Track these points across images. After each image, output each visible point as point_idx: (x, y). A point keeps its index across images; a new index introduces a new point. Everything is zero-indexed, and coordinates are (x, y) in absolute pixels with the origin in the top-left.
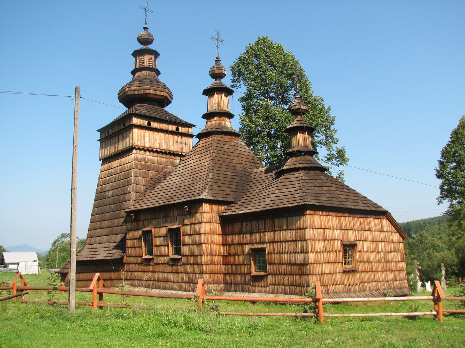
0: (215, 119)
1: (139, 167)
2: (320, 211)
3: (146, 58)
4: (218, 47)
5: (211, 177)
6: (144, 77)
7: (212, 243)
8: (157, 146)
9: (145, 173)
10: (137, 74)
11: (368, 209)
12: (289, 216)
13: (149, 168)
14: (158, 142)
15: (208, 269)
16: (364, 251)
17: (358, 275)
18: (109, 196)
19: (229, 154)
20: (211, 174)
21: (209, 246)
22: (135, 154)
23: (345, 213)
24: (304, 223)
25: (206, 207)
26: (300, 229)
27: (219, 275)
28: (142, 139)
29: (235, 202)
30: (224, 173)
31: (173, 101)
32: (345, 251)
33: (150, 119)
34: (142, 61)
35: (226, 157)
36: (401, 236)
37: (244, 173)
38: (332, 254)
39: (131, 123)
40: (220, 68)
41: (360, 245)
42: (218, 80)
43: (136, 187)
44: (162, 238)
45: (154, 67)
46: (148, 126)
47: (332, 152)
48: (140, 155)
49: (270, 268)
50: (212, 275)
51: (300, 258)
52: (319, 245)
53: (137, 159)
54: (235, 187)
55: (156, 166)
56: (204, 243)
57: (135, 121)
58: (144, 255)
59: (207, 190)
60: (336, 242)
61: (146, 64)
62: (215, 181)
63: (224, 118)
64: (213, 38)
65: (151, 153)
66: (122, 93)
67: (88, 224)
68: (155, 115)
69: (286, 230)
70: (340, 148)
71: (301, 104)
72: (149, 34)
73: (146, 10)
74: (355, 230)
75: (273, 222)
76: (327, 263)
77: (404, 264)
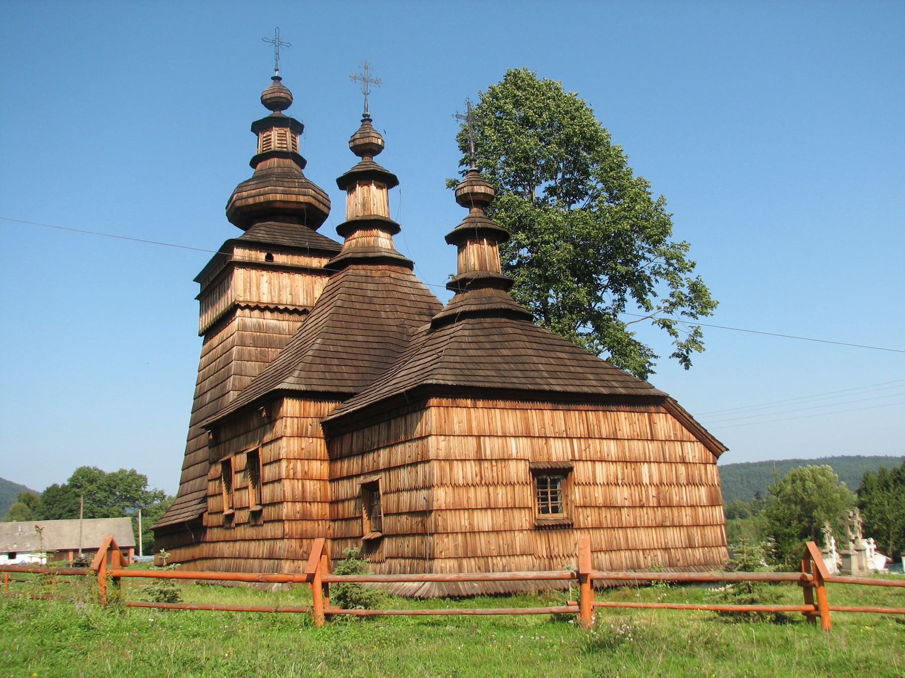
0: (358, 234)
1: (249, 341)
2: (466, 398)
3: (274, 134)
4: (366, 94)
5: (316, 347)
7: (306, 477)
8: (286, 299)
9: (261, 353)
10: (259, 166)
11: (604, 391)
12: (408, 413)
13: (270, 344)
14: (288, 292)
15: (297, 529)
16: (595, 484)
17: (577, 535)
19: (375, 300)
20: (319, 341)
21: (298, 485)
22: (241, 316)
24: (426, 424)
25: (290, 406)
26: (422, 438)
28: (254, 289)
29: (355, 394)
30: (351, 338)
33: (271, 248)
34: (268, 141)
35: (365, 306)
36: (710, 450)
37: (399, 336)
38: (501, 491)
40: (366, 135)
41: (581, 471)
42: (367, 159)
44: (242, 474)
45: (291, 150)
47: (681, 289)
50: (304, 541)
51: (419, 499)
52: (465, 472)
54: (366, 364)
56: (288, 478)
57: (239, 254)
58: (225, 508)
59: (296, 373)
60: (512, 465)
61: (275, 145)
62: (322, 355)
63: (375, 232)
64: (355, 78)
65: (276, 314)
67: (182, 457)
68: (286, 241)
69: (404, 442)
70: (694, 280)
71: (474, 183)
72: (282, 89)
73: (277, 43)
74: (571, 438)
75: (389, 427)
76: (486, 509)
77: (718, 513)
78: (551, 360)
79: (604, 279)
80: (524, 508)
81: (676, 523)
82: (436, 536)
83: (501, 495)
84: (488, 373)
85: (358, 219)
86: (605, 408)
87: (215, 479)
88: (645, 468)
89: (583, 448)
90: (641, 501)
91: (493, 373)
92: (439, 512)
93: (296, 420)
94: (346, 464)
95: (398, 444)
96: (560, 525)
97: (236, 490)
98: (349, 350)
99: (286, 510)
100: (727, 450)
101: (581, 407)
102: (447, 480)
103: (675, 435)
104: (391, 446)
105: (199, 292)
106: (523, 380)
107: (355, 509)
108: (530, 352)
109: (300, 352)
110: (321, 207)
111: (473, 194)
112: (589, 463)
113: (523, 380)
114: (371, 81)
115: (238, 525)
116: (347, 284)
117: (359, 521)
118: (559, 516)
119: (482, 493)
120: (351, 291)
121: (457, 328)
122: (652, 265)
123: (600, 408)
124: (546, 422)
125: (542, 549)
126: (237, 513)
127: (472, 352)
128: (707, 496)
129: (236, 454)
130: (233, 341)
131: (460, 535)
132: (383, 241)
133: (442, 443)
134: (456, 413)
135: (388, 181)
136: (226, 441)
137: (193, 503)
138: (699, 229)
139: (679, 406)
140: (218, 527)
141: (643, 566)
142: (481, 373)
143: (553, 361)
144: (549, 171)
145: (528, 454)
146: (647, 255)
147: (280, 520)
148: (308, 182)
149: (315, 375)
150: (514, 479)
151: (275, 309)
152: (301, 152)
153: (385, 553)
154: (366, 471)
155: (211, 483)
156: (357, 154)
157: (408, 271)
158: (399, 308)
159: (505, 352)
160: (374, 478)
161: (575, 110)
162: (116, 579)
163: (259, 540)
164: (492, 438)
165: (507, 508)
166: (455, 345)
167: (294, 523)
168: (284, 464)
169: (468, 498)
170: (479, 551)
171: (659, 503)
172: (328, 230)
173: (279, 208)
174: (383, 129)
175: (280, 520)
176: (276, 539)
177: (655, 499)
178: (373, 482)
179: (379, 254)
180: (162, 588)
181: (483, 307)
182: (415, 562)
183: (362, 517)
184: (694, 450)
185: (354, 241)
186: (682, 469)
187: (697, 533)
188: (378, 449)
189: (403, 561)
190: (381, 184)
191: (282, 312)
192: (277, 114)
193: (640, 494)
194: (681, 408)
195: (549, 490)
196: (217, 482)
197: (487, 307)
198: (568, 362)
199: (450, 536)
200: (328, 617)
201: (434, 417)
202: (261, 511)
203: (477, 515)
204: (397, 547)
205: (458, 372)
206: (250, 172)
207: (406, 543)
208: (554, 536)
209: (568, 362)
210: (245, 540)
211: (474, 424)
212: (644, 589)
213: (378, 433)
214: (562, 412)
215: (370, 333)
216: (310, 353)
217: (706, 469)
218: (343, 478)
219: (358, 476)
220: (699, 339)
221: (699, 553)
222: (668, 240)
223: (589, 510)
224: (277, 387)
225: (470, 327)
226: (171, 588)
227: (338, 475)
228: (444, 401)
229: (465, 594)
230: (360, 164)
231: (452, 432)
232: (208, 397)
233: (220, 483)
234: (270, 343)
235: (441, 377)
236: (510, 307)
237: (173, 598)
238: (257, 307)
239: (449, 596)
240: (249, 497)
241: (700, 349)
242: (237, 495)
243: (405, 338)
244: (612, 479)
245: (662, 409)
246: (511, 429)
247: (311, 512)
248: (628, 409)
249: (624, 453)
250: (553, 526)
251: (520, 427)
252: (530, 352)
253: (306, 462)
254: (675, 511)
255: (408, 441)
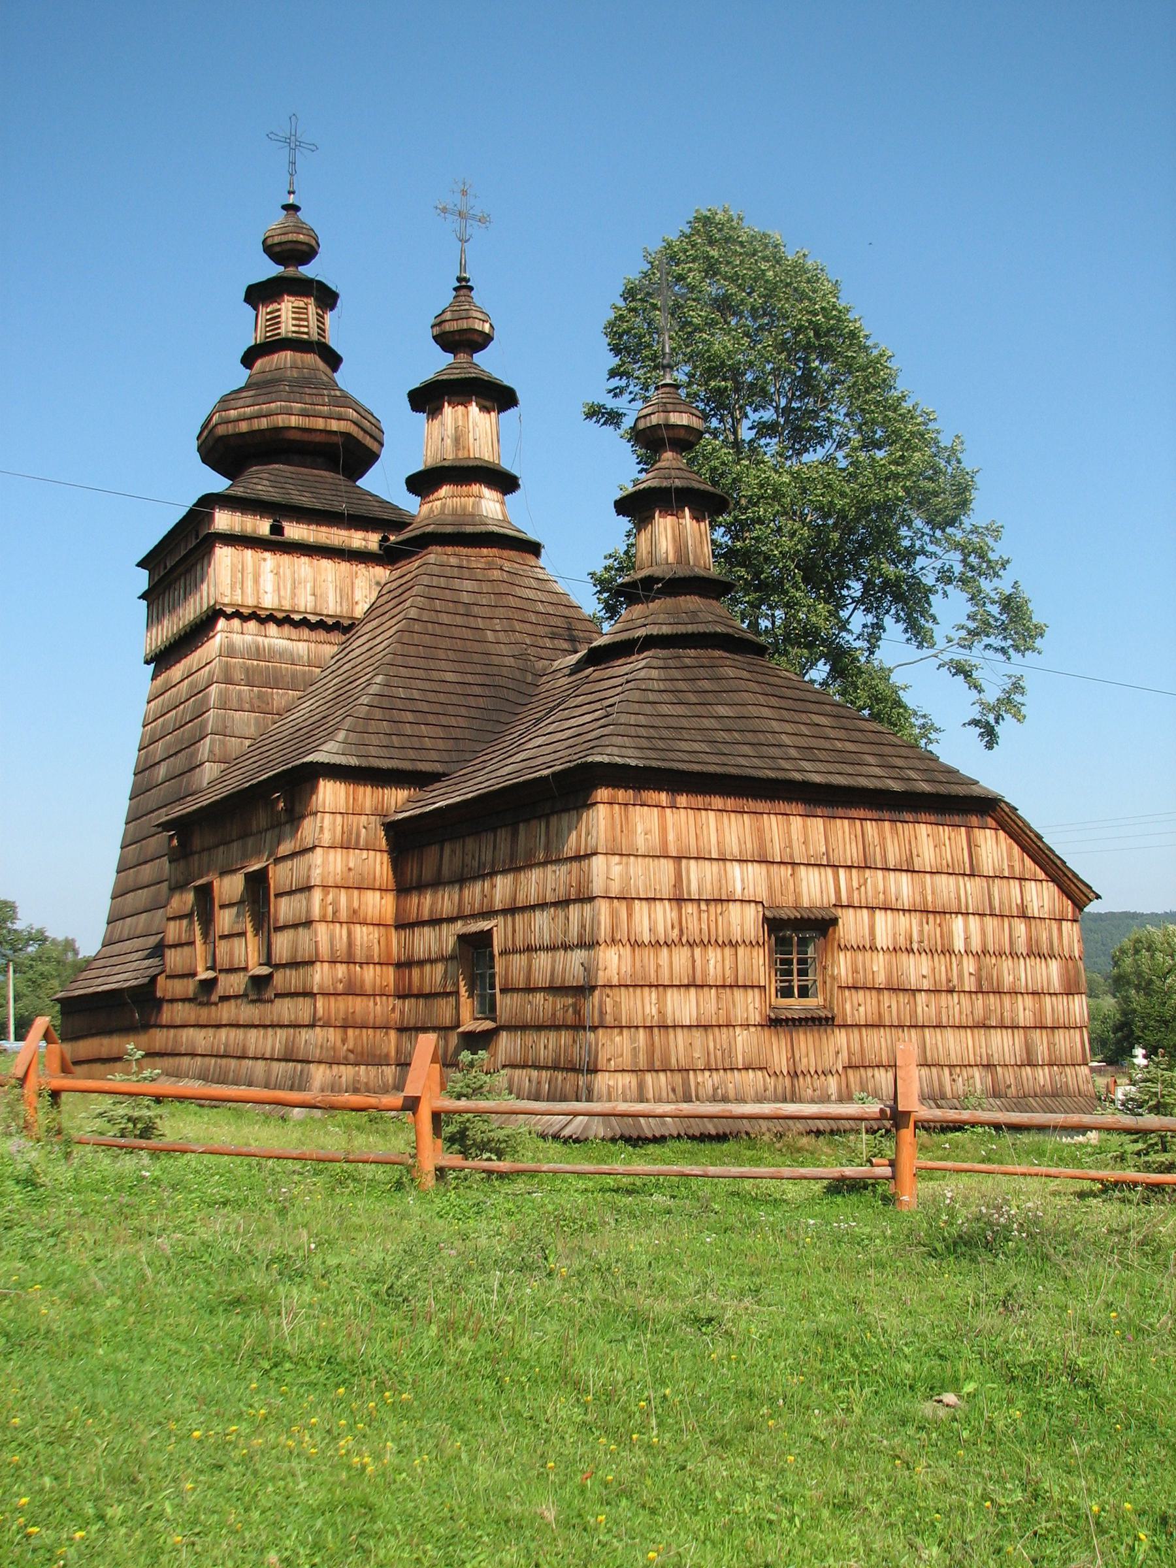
0: (445, 490)
1: (238, 675)
3: (287, 307)
4: (463, 241)
5: (374, 689)
6: (277, 374)
7: (356, 918)
8: (305, 603)
9: (260, 696)
10: (259, 364)
11: (896, 786)
12: (553, 813)
13: (275, 681)
16: (874, 948)
17: (840, 1038)
18: (160, 781)
19: (476, 610)
20: (379, 679)
21: (341, 932)
23: (789, 800)
24: (588, 834)
25: (329, 793)
26: (578, 858)
27: (380, 1034)
28: (249, 584)
29: (445, 775)
30: (435, 675)
31: (385, 453)
32: (782, 944)
34: (275, 320)
35: (459, 620)
36: (1069, 897)
37: (518, 675)
38: (713, 955)
39: (212, 531)
40: (464, 314)
41: (851, 926)
42: (463, 357)
43: (223, 743)
44: (234, 910)
45: (315, 337)
46: (273, 537)
48: (244, 635)
49: (506, 1005)
50: (350, 1031)
51: (572, 964)
53: (230, 651)
54: (462, 722)
55: (304, 673)
56: (323, 920)
57: (223, 520)
58: (200, 969)
59: (341, 736)
60: (734, 909)
61: (287, 327)
62: (385, 704)
63: (475, 488)
64: (444, 210)
66: (205, 434)
68: (305, 500)
69: (544, 864)
70: (1008, 591)
71: (670, 407)
72: (300, 227)
73: (293, 143)
75: (515, 834)
76: (687, 986)
78: (803, 727)
79: (856, 588)
80: (752, 987)
81: (1008, 1023)
82: (600, 1031)
83: (714, 963)
84: (696, 746)
85: (446, 464)
86: (895, 816)
87: (181, 917)
88: (958, 923)
89: (855, 885)
90: (949, 981)
91: (704, 747)
92: (608, 990)
93: (339, 817)
94: (428, 899)
95: (531, 866)
96: (813, 1019)
97: (222, 937)
98: (431, 697)
99: (320, 976)
100: (1098, 897)
101: (854, 813)
102: (622, 935)
103: (1011, 867)
104: (518, 870)
105: (146, 587)
106: (757, 762)
107: (445, 977)
108: (766, 712)
109: (342, 697)
110: (368, 441)
111: (669, 427)
112: (865, 911)
113: (757, 762)
114: (473, 217)
115: (225, 998)
116: (426, 580)
117: (452, 1000)
118: (810, 1002)
119: (681, 957)
120: (435, 593)
121: (638, 664)
122: (938, 564)
123: (887, 815)
124: (794, 837)
125: (779, 1058)
126: (222, 978)
127: (665, 709)
128: (1061, 976)
129: (223, 873)
130: (211, 674)
131: (641, 1031)
132: (489, 505)
133: (616, 866)
134: (642, 816)
135: (499, 398)
136: (203, 850)
137: (135, 956)
138: (1029, 498)
139: (1019, 817)
140: (183, 1000)
141: (949, 1095)
142: (684, 746)
143: (804, 729)
144: (759, 394)
145: (762, 894)
146: (930, 548)
147: (308, 994)
148: (345, 396)
149: (374, 739)
150: (736, 936)
151: (284, 620)
152: (332, 342)
153: (501, 1058)
154: (467, 912)
155: (172, 924)
156: (446, 347)
157: (531, 559)
158: (518, 626)
159: (722, 710)
160: (484, 925)
161: (798, 282)
162: (55, 1095)
163: (265, 1027)
164: (700, 861)
165: (724, 986)
166: (636, 695)
167: (332, 999)
168: (317, 895)
169: (658, 966)
170: (673, 1061)
171: (980, 985)
172: (385, 482)
173: (320, 443)
174: (492, 307)
175: (308, 994)
176: (300, 1026)
177: (973, 978)
178: (482, 932)
179: (483, 529)
180: (131, 1113)
181: (682, 629)
182: (560, 1076)
183: (457, 993)
184: (1042, 896)
185: (438, 503)
186: (1021, 927)
187: (1040, 1040)
188: (493, 874)
189: (535, 1073)
190: (488, 404)
191: (296, 624)
192: (291, 271)
193: (949, 969)
194: (1024, 821)
195: (795, 957)
196: (185, 922)
197: (690, 629)
198: (832, 733)
199: (625, 1031)
200: (441, 1172)
201: (602, 823)
202: (270, 976)
203: (672, 996)
204: (524, 1046)
205: (644, 743)
206: (241, 376)
207: (543, 1041)
208: (802, 1037)
209: (832, 733)
210: (238, 1026)
211: (671, 837)
212: (950, 1135)
213: (484, 849)
214: (820, 820)
215: (469, 668)
216: (365, 700)
217: (1060, 929)
218: (422, 924)
219: (451, 920)
220: (1017, 698)
221: (1043, 1076)
222: (967, 522)
223: (861, 993)
224: (305, 760)
225: (660, 663)
226: (146, 1113)
227: (413, 917)
228: (621, 795)
229: (650, 1135)
230: (451, 367)
231: (631, 845)
232: (162, 771)
233: (191, 923)
234: (276, 680)
235: (616, 751)
236: (730, 631)
237: (147, 1131)
238: (254, 616)
239: (622, 1137)
240: (247, 952)
241: (1019, 718)
242: (222, 947)
243: (529, 678)
244: (902, 942)
245: (991, 822)
246: (733, 848)
247: (363, 982)
248: (933, 818)
249: (924, 897)
250: (800, 1019)
251: (749, 845)
252: (766, 712)
253: (356, 892)
254: (1007, 999)
255: (552, 862)
